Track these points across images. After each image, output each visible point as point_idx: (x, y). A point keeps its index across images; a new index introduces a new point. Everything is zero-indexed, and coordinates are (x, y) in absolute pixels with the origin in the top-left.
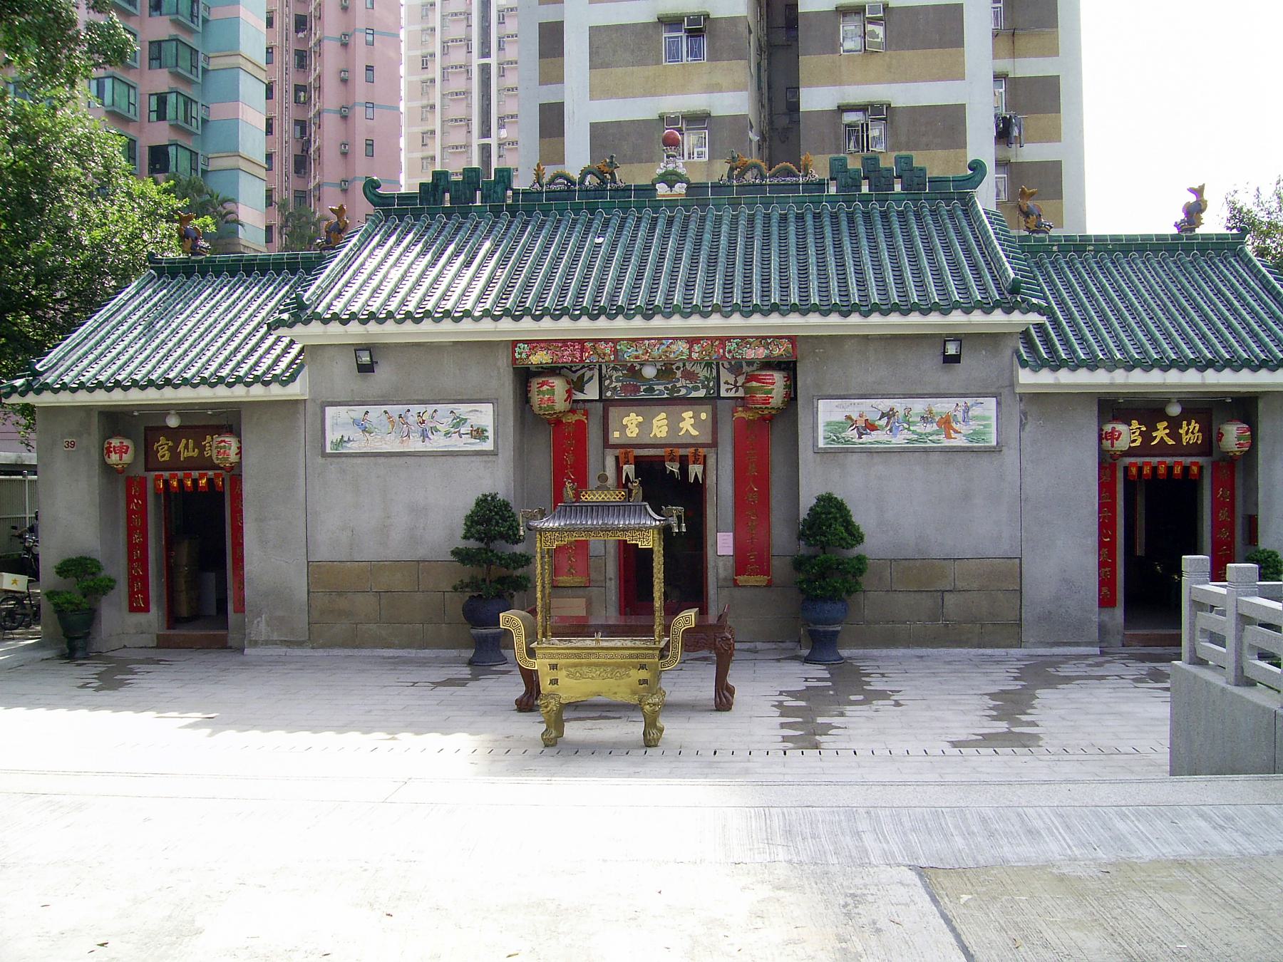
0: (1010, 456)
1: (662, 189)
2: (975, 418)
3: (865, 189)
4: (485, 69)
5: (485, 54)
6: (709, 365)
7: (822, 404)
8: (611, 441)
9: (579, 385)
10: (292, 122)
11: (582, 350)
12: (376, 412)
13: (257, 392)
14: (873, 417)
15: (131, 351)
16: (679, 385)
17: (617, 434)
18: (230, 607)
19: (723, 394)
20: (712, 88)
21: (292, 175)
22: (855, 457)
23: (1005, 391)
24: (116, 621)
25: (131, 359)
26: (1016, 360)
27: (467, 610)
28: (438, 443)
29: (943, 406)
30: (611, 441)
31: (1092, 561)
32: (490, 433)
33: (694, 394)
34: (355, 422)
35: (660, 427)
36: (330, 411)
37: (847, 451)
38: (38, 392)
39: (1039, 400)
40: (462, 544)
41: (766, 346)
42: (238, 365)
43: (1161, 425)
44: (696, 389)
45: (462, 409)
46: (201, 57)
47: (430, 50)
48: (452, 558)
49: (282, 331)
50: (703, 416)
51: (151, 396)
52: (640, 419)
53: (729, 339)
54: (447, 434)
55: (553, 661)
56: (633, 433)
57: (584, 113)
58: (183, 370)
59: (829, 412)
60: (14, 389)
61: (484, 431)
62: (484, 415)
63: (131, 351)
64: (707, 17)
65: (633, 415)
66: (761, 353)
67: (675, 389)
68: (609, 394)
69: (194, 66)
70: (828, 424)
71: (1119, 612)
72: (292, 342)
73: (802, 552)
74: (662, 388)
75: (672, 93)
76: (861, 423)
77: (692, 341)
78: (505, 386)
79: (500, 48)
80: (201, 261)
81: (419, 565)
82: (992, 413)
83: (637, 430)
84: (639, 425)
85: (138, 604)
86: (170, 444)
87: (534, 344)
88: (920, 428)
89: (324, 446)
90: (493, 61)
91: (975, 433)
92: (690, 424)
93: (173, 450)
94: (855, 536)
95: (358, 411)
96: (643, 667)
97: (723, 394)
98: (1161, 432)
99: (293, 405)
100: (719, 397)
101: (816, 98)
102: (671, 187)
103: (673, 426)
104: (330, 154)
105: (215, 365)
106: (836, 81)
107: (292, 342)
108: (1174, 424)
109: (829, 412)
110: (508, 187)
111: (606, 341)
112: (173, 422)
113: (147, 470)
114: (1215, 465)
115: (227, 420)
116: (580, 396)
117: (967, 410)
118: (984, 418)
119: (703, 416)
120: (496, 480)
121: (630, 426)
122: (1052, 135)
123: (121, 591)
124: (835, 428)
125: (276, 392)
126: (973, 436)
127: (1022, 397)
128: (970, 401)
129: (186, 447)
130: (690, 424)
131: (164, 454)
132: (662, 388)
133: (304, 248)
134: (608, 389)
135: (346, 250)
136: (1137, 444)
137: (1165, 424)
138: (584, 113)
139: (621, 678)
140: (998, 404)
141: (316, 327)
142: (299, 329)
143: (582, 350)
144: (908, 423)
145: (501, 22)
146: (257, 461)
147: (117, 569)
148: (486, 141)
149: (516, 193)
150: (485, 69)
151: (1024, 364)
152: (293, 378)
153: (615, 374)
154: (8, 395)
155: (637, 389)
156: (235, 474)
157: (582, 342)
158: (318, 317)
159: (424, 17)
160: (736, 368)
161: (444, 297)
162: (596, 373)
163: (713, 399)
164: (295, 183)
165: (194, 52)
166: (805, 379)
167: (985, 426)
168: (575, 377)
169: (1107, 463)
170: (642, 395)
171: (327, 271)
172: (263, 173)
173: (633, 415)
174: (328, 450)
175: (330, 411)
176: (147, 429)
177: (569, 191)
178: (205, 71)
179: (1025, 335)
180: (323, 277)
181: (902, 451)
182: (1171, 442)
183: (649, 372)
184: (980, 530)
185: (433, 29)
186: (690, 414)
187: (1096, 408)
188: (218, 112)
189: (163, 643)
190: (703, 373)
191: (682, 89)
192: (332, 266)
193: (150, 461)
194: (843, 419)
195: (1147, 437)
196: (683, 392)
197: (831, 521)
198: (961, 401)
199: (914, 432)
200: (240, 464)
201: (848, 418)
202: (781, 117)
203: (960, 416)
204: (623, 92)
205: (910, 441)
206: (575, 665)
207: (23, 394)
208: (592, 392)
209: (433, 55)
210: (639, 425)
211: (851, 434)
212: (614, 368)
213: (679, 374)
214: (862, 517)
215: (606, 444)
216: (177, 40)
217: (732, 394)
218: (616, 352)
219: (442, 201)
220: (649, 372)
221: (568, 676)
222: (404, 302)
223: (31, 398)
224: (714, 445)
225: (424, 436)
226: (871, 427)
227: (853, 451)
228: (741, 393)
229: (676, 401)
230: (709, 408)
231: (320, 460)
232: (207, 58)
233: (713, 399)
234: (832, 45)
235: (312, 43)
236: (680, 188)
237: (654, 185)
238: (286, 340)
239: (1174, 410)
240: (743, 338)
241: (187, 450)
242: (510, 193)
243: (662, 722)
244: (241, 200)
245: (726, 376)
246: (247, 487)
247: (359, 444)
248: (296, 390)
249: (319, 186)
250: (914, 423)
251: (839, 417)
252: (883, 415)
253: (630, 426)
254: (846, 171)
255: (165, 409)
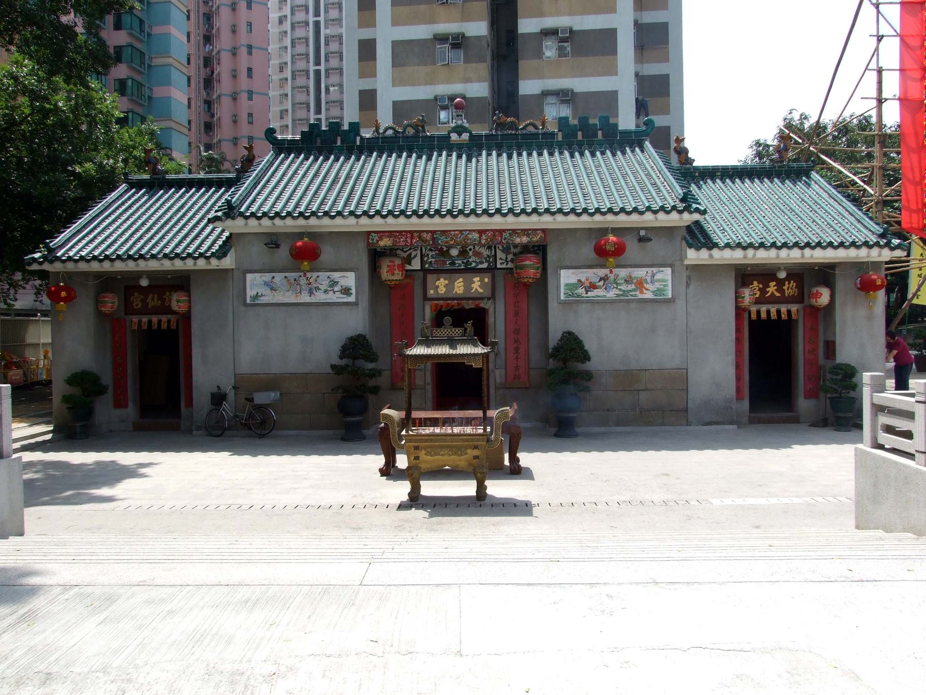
0: (680, 304)
1: (454, 136)
2: (658, 281)
3: (580, 137)
4: (318, 73)
5: (318, 63)
6: (489, 248)
7: (563, 272)
8: (429, 296)
9: (408, 260)
10: (202, 102)
11: (412, 238)
12: (279, 277)
13: (201, 264)
14: (595, 280)
15: (117, 231)
16: (471, 260)
17: (432, 292)
18: (183, 403)
19: (499, 266)
20: (467, 80)
21: (203, 134)
22: (584, 306)
23: (677, 263)
24: (104, 411)
25: (115, 241)
26: (684, 243)
27: (339, 407)
28: (320, 297)
29: (640, 273)
30: (429, 296)
31: (732, 370)
32: (353, 291)
33: (480, 266)
34: (266, 284)
35: (459, 287)
36: (249, 277)
37: (578, 302)
38: (51, 262)
39: (698, 269)
40: (336, 360)
41: (528, 235)
42: (188, 246)
43: (773, 284)
44: (482, 263)
45: (336, 275)
46: (147, 57)
47: (285, 61)
48: (331, 371)
49: (217, 224)
50: (486, 280)
51: (131, 266)
52: (447, 282)
53: (504, 231)
54: (326, 291)
55: (416, 444)
56: (442, 290)
57: (389, 93)
58: (151, 249)
59: (567, 277)
60: (34, 260)
61: (349, 289)
62: (349, 279)
63: (117, 231)
64: (463, 35)
65: (442, 280)
66: (525, 240)
67: (468, 263)
68: (427, 266)
69: (142, 63)
70: (567, 285)
71: (746, 403)
72: (223, 231)
73: (551, 367)
74: (460, 262)
75: (442, 83)
76: (587, 284)
77: (481, 232)
78: (363, 260)
79: (327, 60)
80: (159, 179)
81: (304, 378)
82: (669, 278)
83: (444, 289)
84: (446, 286)
85: (120, 403)
86: (142, 297)
87: (381, 234)
88: (624, 287)
89: (245, 299)
90: (322, 68)
91: (658, 290)
92: (477, 285)
93: (144, 301)
94: (585, 356)
95: (267, 277)
96: (476, 447)
97: (499, 266)
98: (772, 288)
99: (225, 271)
100: (496, 268)
101: (528, 87)
102: (460, 135)
103: (468, 286)
104: (226, 122)
105: (172, 245)
106: (541, 76)
107: (223, 231)
108: (780, 283)
109: (567, 277)
110: (358, 134)
111: (427, 232)
112: (144, 283)
113: (126, 314)
114: (804, 308)
115: (181, 282)
116: (408, 267)
117: (653, 275)
118: (664, 281)
119: (486, 280)
120: (356, 322)
121: (440, 286)
122: (665, 110)
123: (109, 396)
124: (571, 287)
125: (214, 263)
126: (659, 291)
127: (688, 267)
128: (655, 270)
129: (153, 299)
130: (477, 285)
131: (137, 303)
132: (460, 262)
133: (222, 173)
134: (426, 262)
135: (256, 172)
136: (757, 296)
137: (774, 283)
138: (389, 93)
139: (461, 455)
140: (673, 272)
141: (240, 221)
142: (229, 222)
143: (412, 238)
144: (617, 284)
145: (327, 44)
146: (201, 309)
147: (107, 379)
148: (319, 116)
149: (362, 139)
150: (318, 73)
151: (690, 246)
152: (225, 255)
153: (431, 253)
154: (30, 264)
155: (444, 263)
156: (186, 318)
157: (411, 232)
158: (242, 215)
159: (281, 40)
160: (506, 250)
161: (322, 203)
162: (419, 252)
163: (492, 270)
164: (205, 139)
165: (142, 54)
166: (552, 257)
167: (665, 286)
168: (405, 255)
169: (740, 311)
170: (448, 266)
171: (246, 185)
172: (186, 131)
173: (442, 280)
174: (248, 301)
175: (249, 277)
176: (126, 287)
177: (396, 137)
178: (149, 66)
179: (688, 228)
180: (243, 189)
181: (612, 302)
182: (778, 295)
183: (454, 252)
184: (662, 351)
185: (286, 48)
186: (478, 279)
187: (733, 274)
188: (159, 92)
189: (138, 428)
190: (485, 252)
191: (448, 81)
192: (248, 182)
193: (129, 309)
194: (576, 281)
195: (763, 291)
196: (474, 265)
197: (571, 348)
198: (650, 270)
199: (620, 290)
200: (189, 312)
201: (579, 281)
202: (505, 98)
203: (649, 279)
204: (413, 82)
205: (618, 295)
206: (430, 447)
207: (41, 263)
208: (416, 265)
209: (286, 63)
210: (446, 286)
211: (581, 291)
212: (430, 250)
213: (471, 253)
214: (590, 345)
215: (426, 298)
216: (132, 46)
217: (504, 266)
218: (433, 239)
219: (316, 143)
220: (454, 252)
221: (426, 454)
222: (297, 205)
223: (46, 267)
224: (493, 297)
225: (311, 293)
226: (593, 286)
227: (582, 302)
228: (510, 265)
229: (470, 271)
230: (489, 275)
231: (243, 308)
232: (151, 58)
233: (492, 270)
234: (539, 54)
235: (214, 53)
236: (465, 136)
237: (449, 134)
238: (219, 230)
239: (782, 275)
240: (514, 231)
241: (153, 301)
242: (358, 138)
243: (487, 483)
244: (173, 147)
245: (500, 254)
246: (195, 326)
247: (269, 297)
248: (228, 262)
249: (220, 141)
250: (621, 284)
251: (573, 280)
252: (601, 279)
253: (440, 286)
254: (569, 125)
255: (139, 274)
